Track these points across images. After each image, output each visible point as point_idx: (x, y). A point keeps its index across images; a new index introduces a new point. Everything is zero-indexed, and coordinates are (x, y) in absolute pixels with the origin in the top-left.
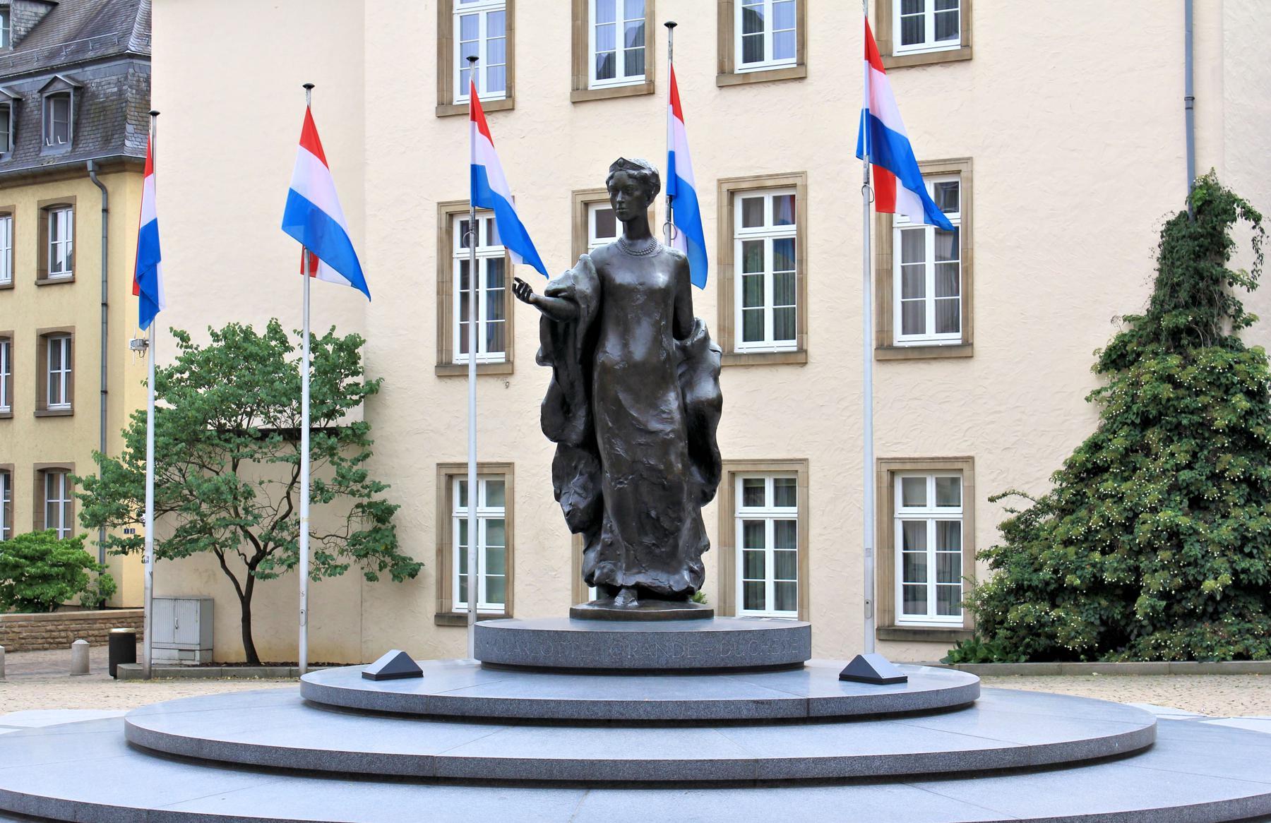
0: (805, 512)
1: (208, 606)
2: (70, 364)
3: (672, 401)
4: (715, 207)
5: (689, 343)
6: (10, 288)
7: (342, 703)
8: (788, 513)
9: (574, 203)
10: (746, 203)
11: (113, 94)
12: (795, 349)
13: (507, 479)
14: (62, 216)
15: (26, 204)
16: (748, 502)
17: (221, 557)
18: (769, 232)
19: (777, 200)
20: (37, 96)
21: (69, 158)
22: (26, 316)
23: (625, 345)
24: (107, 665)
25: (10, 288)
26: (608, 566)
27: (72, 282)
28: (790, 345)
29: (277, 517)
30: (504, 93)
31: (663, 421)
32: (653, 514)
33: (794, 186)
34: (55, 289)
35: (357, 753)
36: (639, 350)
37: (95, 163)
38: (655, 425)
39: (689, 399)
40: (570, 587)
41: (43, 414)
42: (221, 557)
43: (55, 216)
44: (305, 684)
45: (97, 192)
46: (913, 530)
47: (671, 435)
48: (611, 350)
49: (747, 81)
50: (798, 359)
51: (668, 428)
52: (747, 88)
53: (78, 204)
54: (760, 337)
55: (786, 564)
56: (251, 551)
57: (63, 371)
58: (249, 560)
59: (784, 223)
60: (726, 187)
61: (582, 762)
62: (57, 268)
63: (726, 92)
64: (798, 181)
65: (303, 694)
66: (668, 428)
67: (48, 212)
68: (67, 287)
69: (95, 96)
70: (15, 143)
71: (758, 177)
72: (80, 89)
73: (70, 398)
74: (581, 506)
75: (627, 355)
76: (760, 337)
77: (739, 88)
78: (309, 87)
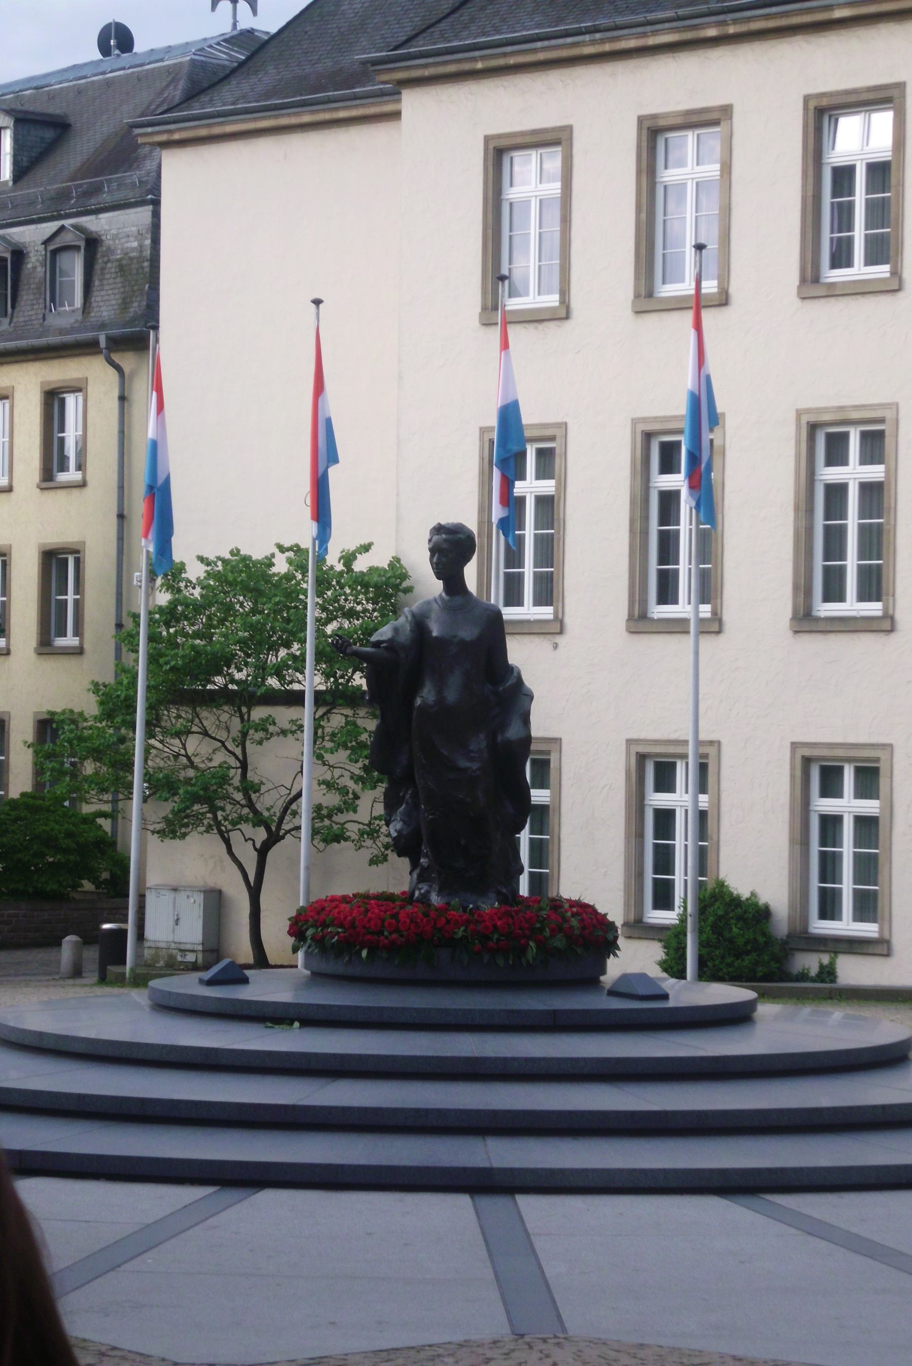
0: (890, 807)
1: (215, 903)
2: (78, 589)
3: (479, 743)
4: (793, 442)
5: (501, 689)
6: (9, 489)
7: (172, 1004)
8: (870, 807)
9: (634, 432)
10: (830, 437)
11: (133, 249)
12: (880, 613)
13: (553, 758)
14: (72, 402)
15: (28, 382)
16: (659, 788)
17: (227, 842)
18: (854, 472)
19: (864, 435)
20: (42, 248)
21: (79, 330)
22: (27, 523)
23: (440, 692)
24: (96, 966)
25: (9, 489)
26: (424, 887)
27: (83, 485)
28: (874, 608)
29: (291, 796)
30: (556, 297)
31: (472, 759)
32: (463, 842)
33: (882, 421)
34: (61, 494)
35: (159, 1045)
36: (452, 695)
37: (109, 339)
38: (463, 763)
39: (499, 738)
40: (622, 886)
41: (45, 646)
42: (227, 842)
43: (62, 402)
44: (154, 990)
45: (112, 373)
46: (836, 492)
47: (478, 773)
48: (426, 695)
49: (834, 292)
50: (885, 625)
51: (475, 766)
52: (832, 300)
53: (90, 389)
54: (841, 598)
55: (868, 868)
56: (261, 835)
57: (70, 597)
58: (258, 846)
59: (872, 462)
60: (805, 419)
61: (334, 1056)
62: (63, 468)
63: (809, 304)
64: (888, 414)
65: (150, 999)
66: (475, 766)
67: (53, 400)
68: (75, 492)
69: (110, 251)
70: (13, 307)
71: (841, 408)
72: (92, 243)
73: (78, 632)
74: (405, 833)
75: (440, 700)
76: (841, 598)
77: (823, 301)
78: (317, 302)
